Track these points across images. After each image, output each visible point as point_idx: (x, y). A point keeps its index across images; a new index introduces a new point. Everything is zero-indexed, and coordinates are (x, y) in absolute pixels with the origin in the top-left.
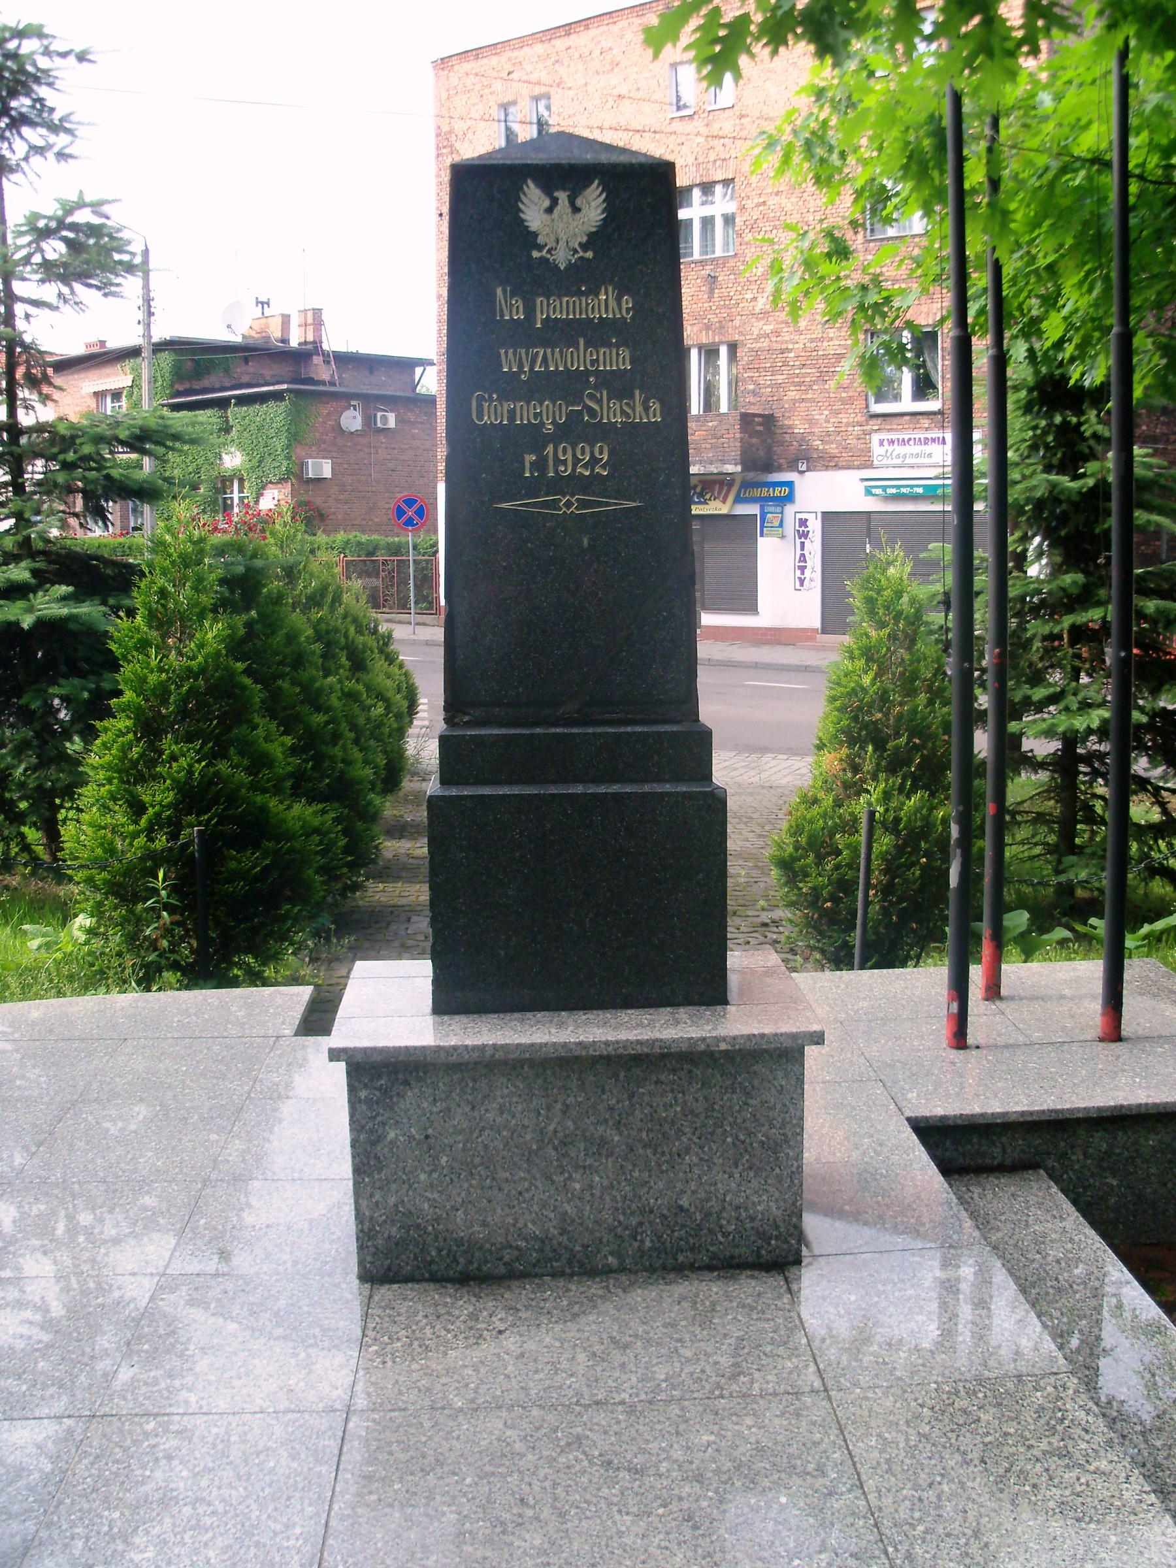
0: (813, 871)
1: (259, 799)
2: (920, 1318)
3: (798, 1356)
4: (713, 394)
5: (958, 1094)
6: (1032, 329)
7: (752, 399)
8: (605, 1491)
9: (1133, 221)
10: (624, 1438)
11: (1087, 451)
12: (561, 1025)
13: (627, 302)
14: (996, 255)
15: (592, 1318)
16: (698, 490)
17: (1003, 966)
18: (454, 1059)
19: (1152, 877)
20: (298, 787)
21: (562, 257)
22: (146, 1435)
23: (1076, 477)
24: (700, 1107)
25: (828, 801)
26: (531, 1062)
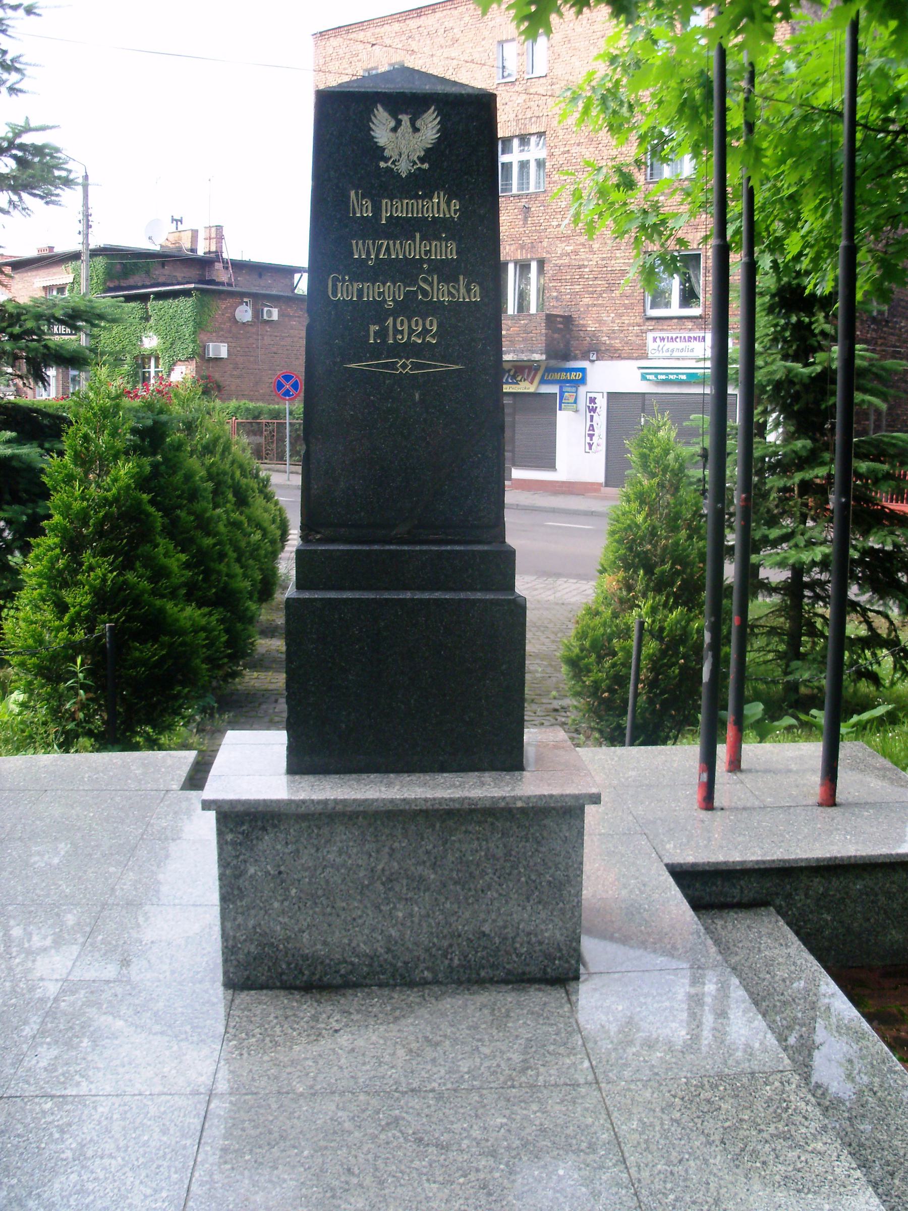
0: (595, 668)
1: (158, 602)
2: (674, 1025)
3: (575, 1055)
4: (524, 301)
5: (706, 846)
6: (777, 245)
7: (555, 304)
8: (417, 1164)
9: (859, 160)
10: (434, 1120)
11: (816, 344)
12: (389, 785)
13: (455, 204)
14: (751, 184)
15: (410, 1021)
16: (512, 373)
17: (743, 746)
18: (303, 810)
19: (859, 679)
20: (192, 594)
21: (404, 168)
22: (44, 1113)
23: (807, 365)
24: (500, 853)
25: (608, 613)
26: (364, 814)
